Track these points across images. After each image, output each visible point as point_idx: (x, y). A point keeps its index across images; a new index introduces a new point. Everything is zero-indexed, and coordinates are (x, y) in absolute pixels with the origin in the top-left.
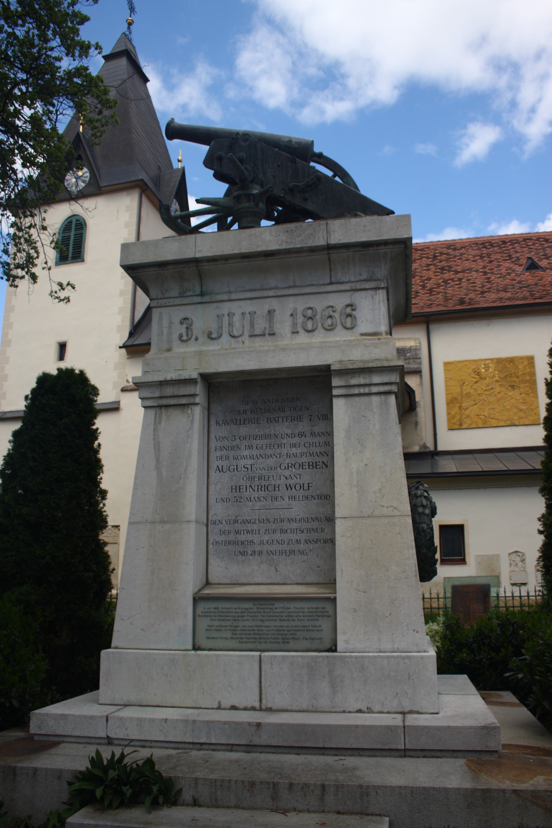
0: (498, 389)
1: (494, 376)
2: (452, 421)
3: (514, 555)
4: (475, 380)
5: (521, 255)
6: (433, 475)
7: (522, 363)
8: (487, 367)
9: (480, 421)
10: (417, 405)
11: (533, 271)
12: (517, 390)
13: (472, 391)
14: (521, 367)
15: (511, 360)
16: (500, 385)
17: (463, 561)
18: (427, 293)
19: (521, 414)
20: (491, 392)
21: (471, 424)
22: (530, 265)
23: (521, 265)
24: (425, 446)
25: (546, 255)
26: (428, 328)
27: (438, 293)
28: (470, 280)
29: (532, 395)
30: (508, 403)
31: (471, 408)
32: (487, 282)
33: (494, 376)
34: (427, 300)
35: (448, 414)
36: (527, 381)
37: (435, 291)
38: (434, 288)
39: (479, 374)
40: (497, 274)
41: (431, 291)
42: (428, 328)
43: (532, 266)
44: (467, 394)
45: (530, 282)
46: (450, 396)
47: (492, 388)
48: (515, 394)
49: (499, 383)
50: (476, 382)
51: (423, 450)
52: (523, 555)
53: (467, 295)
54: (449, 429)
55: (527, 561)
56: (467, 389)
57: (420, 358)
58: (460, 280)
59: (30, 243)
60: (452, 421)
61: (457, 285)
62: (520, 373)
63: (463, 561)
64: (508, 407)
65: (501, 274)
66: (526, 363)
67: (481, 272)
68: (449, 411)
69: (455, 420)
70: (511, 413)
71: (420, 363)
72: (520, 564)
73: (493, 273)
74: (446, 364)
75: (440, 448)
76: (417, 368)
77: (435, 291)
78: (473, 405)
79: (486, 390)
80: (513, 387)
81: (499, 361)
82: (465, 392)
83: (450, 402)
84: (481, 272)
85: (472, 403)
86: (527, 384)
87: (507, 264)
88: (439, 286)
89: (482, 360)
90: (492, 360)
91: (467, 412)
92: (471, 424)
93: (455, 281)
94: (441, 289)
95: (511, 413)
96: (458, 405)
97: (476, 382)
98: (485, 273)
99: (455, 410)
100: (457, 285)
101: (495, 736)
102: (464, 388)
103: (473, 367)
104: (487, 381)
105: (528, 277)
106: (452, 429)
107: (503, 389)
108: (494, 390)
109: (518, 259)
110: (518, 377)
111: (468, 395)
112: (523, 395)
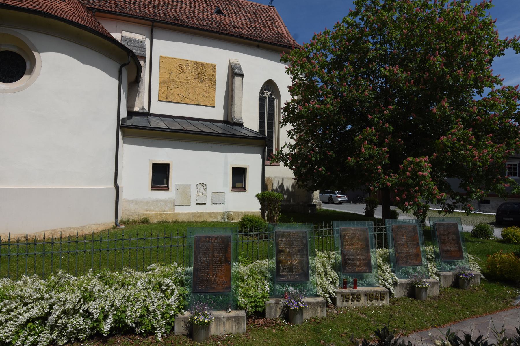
0: (192, 80)
1: (191, 72)
2: (162, 96)
3: (200, 186)
4: (180, 72)
5: (213, 4)
6: (151, 129)
7: (209, 68)
8: (187, 65)
9: (179, 98)
10: (141, 79)
11: (220, 15)
12: (204, 84)
13: (177, 79)
14: (208, 70)
15: (203, 65)
16: (194, 79)
17: (167, 188)
18: (153, 8)
19: (205, 99)
20: (188, 81)
21: (173, 100)
22: (218, 11)
23: (213, 9)
24: (143, 108)
25: (227, 8)
26: (152, 33)
27: (161, 10)
28: (182, 8)
29: (212, 88)
30: (198, 90)
31: (174, 89)
32: (192, 13)
33: (191, 72)
34: (153, 12)
35: (159, 90)
36: (210, 79)
37: (158, 8)
38: (158, 6)
39: (182, 68)
40: (198, 10)
41: (156, 7)
42: (152, 33)
43: (219, 12)
44: (173, 80)
45: (217, 20)
46: (162, 79)
47: (189, 80)
48: (202, 85)
49: (193, 77)
50: (180, 74)
51: (142, 111)
52: (206, 186)
53: (179, 16)
54: (159, 101)
55: (207, 190)
56: (173, 77)
57: (145, 48)
58: (175, 6)
59: (351, 297)
60: (162, 96)
61: (173, 8)
62: (207, 74)
63: (167, 188)
64: (197, 93)
65: (201, 10)
66: (211, 68)
67: (189, 6)
68: (160, 89)
69: (163, 95)
70: (199, 97)
71: (145, 52)
72: (203, 191)
73: (195, 8)
74: (161, 57)
75: (152, 112)
76: (143, 54)
77: (158, 8)
78: (176, 88)
79: (185, 80)
80: (202, 81)
81: (196, 63)
82: (171, 78)
83: (162, 83)
84: (189, 6)
85: (176, 86)
86: (210, 81)
87: (205, 6)
88: (161, 6)
89: (185, 60)
90: (191, 61)
91: (172, 91)
92: (173, 100)
93: (172, 6)
94: (162, 8)
95: (199, 97)
96: (166, 86)
97: (180, 74)
98: (191, 7)
99: (164, 89)
100: (173, 8)
101: (158, 248)
102: (172, 75)
103: (179, 63)
104: (187, 74)
105: (216, 17)
106: (161, 101)
107: (196, 81)
108: (190, 81)
109: (211, 5)
110: (205, 76)
111: (174, 80)
112: (207, 87)
